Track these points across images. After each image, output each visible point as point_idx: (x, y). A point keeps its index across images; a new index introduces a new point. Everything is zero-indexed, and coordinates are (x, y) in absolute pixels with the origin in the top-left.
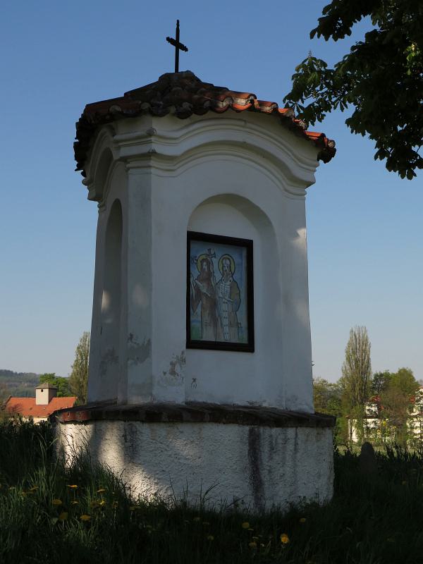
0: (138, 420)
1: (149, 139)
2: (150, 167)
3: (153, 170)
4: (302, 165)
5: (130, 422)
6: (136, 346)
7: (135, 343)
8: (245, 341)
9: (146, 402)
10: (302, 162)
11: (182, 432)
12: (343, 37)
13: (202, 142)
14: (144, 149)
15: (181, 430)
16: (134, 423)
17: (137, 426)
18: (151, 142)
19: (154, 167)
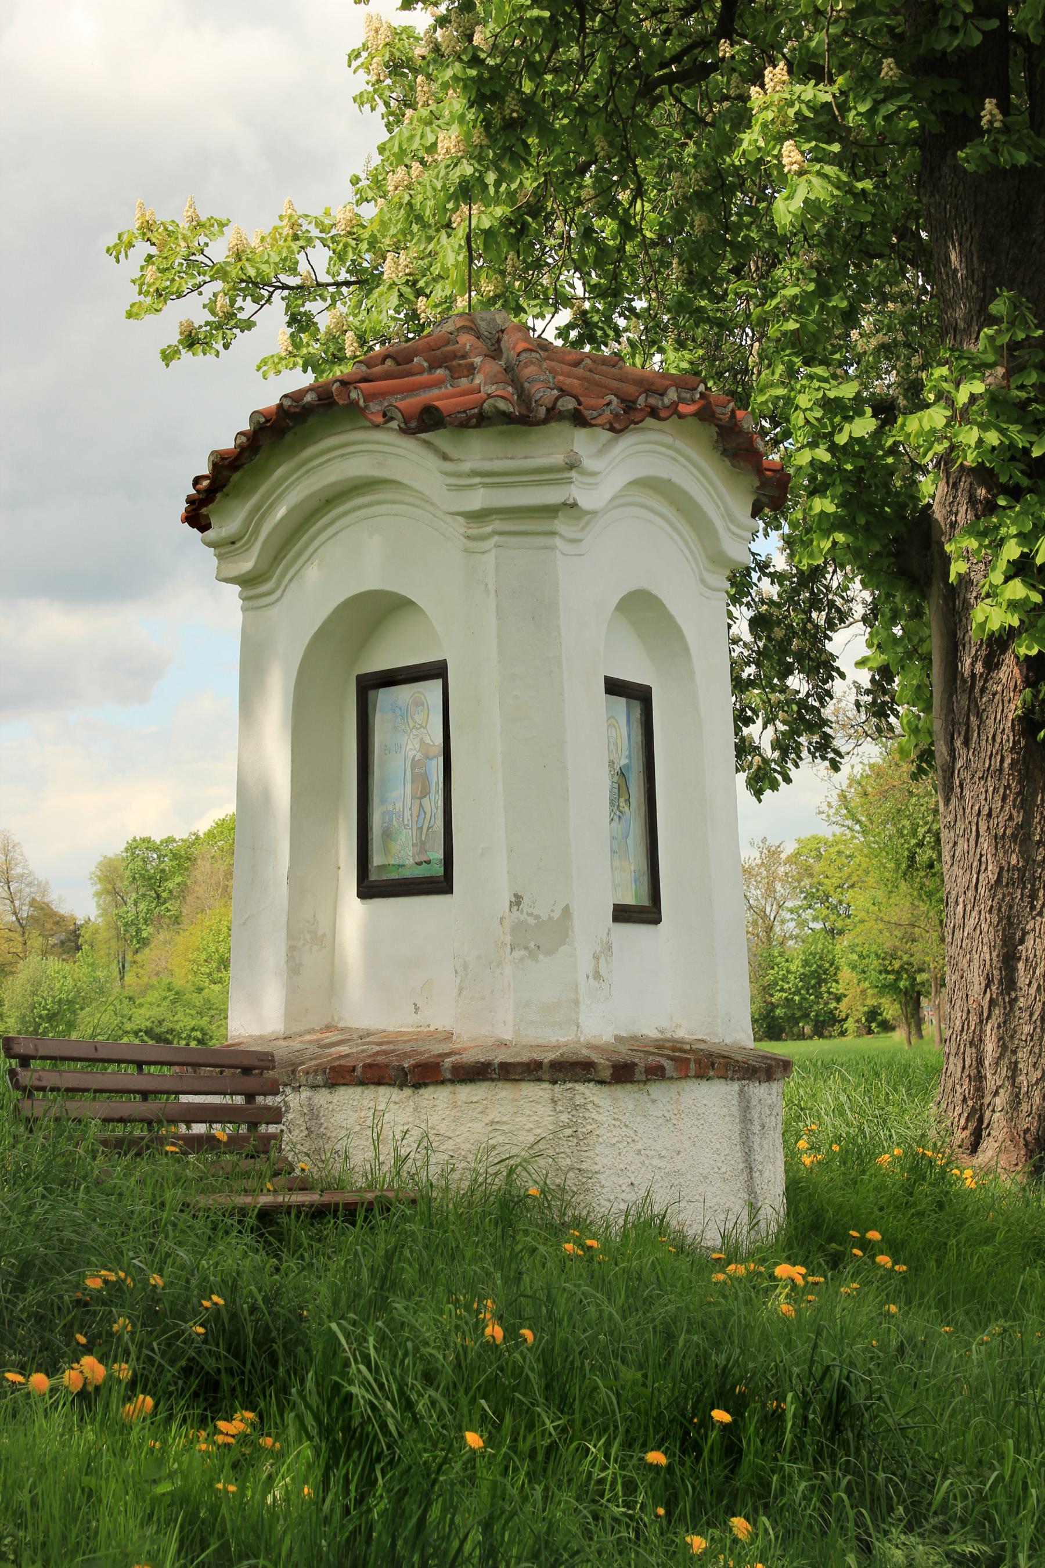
0: (589, 1081)
1: (566, 475)
2: (553, 533)
3: (558, 541)
4: (732, 528)
5: (569, 1085)
6: (531, 921)
7: (529, 914)
8: (645, 902)
9: (562, 1039)
10: (739, 526)
11: (654, 1101)
12: (289, 324)
13: (397, 506)
14: (552, 496)
15: (653, 1097)
16: (580, 1087)
17: (588, 1094)
18: (569, 482)
19: (561, 536)
